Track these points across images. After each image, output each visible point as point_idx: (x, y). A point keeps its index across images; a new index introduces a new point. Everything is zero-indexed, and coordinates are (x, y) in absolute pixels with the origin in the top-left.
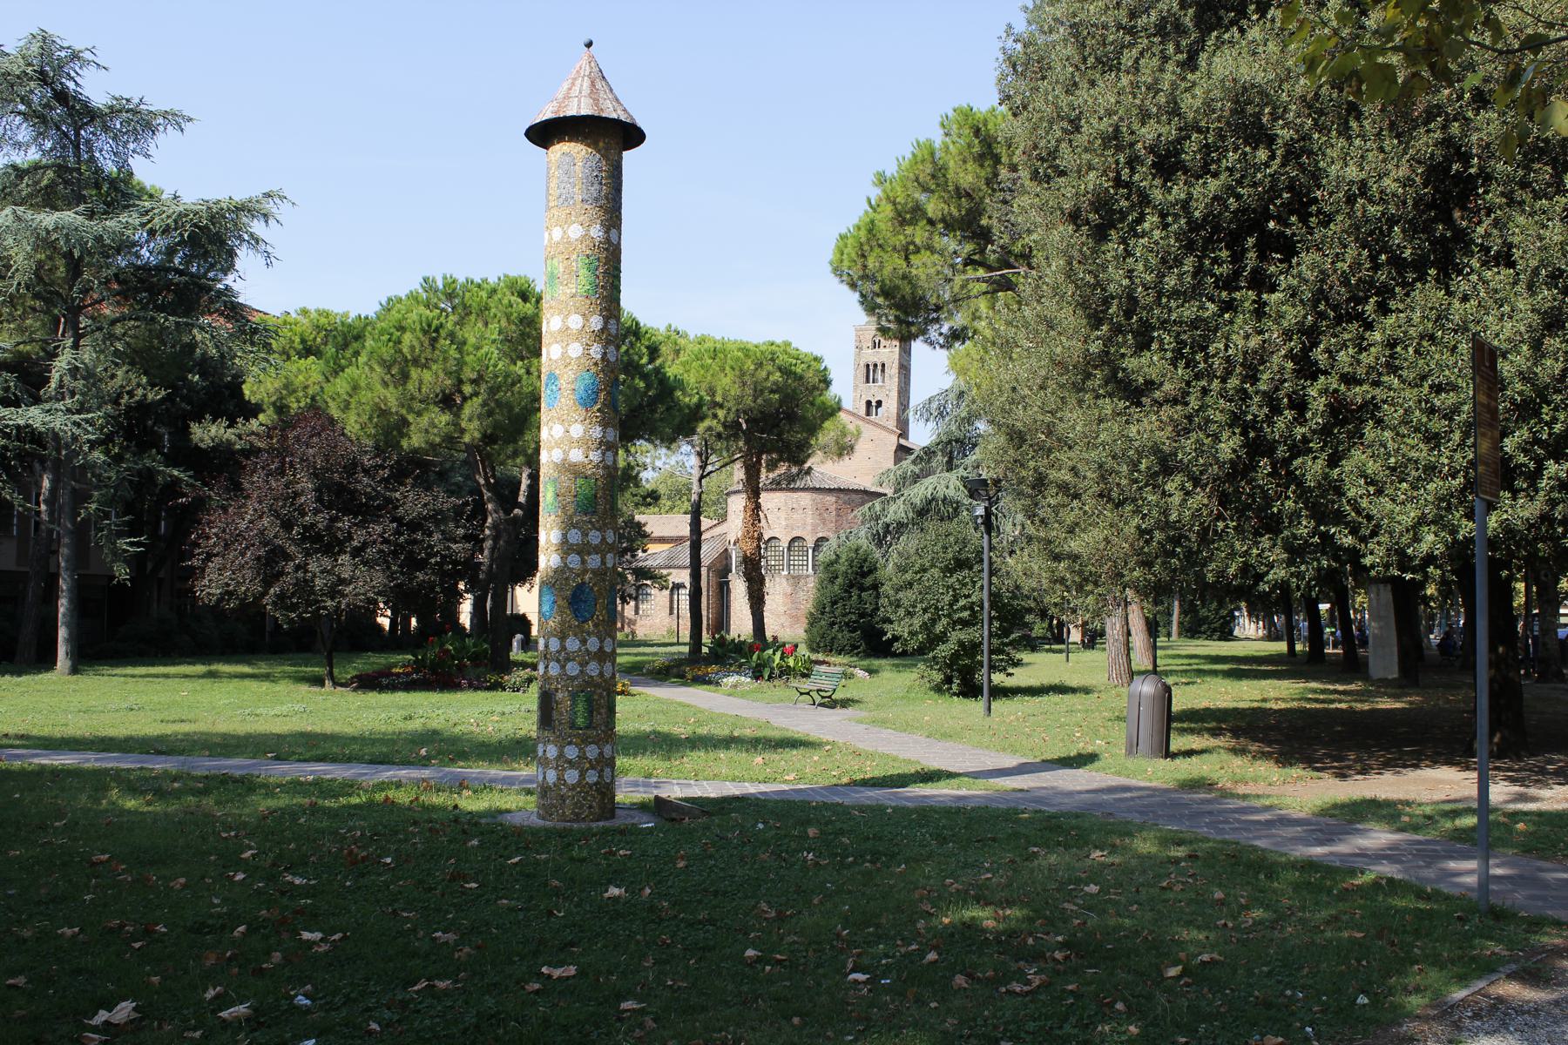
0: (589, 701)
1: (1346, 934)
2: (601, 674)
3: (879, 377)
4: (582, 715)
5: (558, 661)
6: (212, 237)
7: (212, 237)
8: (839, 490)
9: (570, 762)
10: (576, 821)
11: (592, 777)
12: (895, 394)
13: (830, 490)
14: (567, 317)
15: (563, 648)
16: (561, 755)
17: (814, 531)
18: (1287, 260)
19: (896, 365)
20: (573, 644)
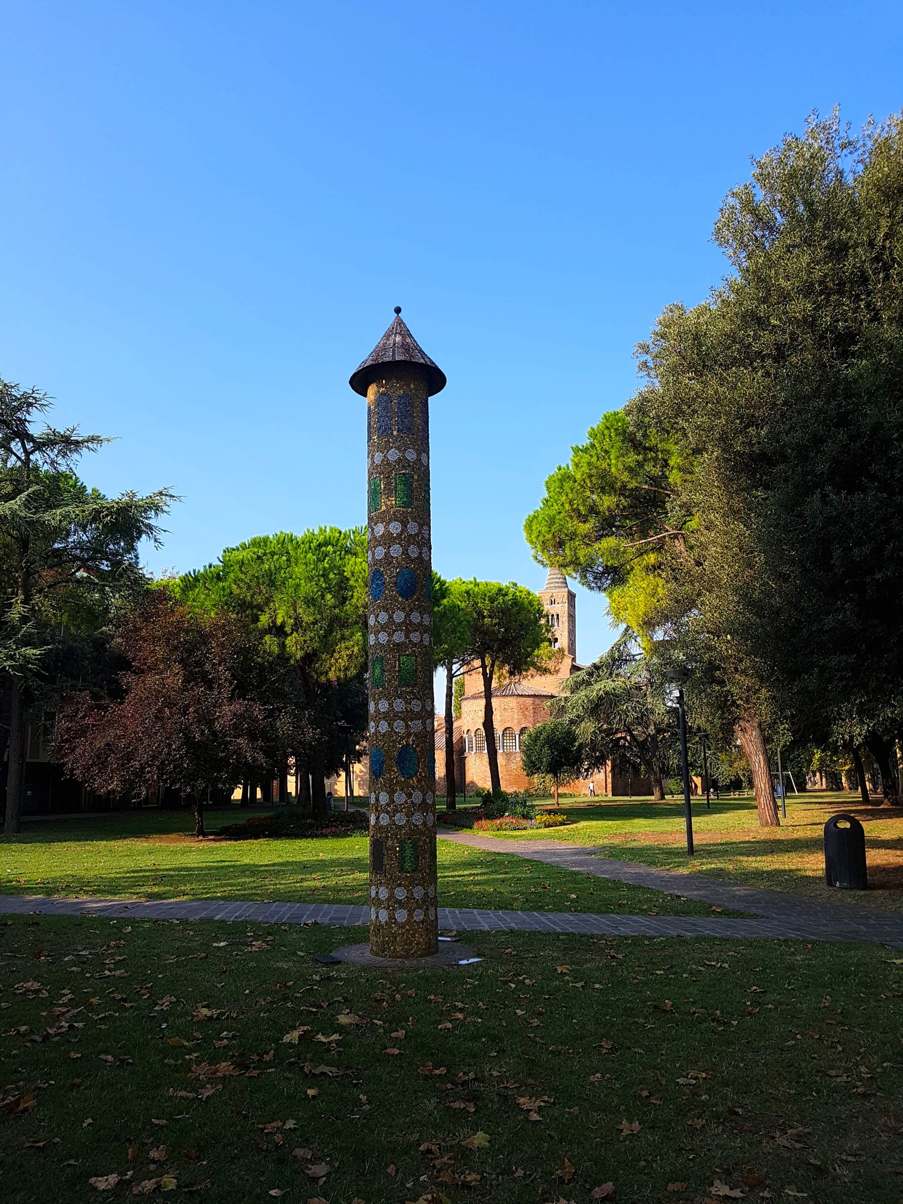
0: (415, 847)
1: (707, 932)
2: (425, 824)
3: (556, 624)
4: (407, 858)
5: (388, 812)
6: (126, 523)
7: (126, 523)
8: (535, 696)
9: (399, 902)
10: (407, 957)
11: (419, 916)
12: (566, 633)
13: (529, 696)
14: (388, 524)
15: (392, 801)
16: (392, 896)
17: (519, 723)
18: (512, 673)
19: (566, 615)
20: (400, 798)
